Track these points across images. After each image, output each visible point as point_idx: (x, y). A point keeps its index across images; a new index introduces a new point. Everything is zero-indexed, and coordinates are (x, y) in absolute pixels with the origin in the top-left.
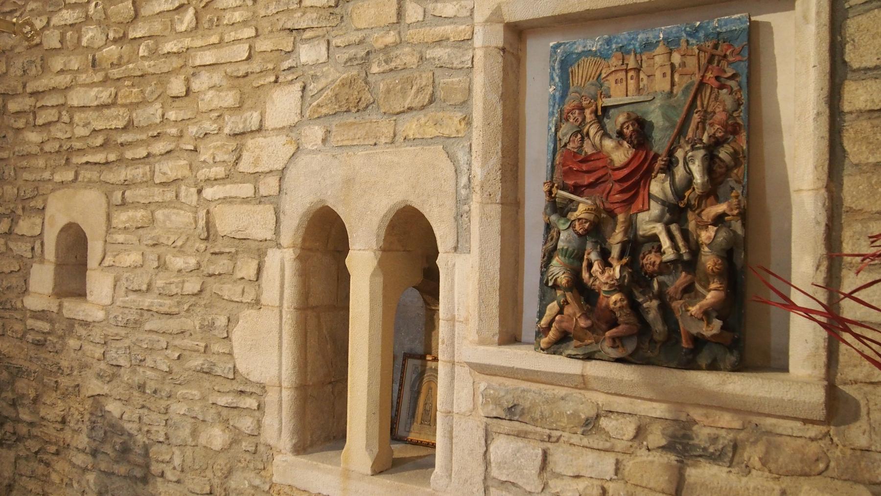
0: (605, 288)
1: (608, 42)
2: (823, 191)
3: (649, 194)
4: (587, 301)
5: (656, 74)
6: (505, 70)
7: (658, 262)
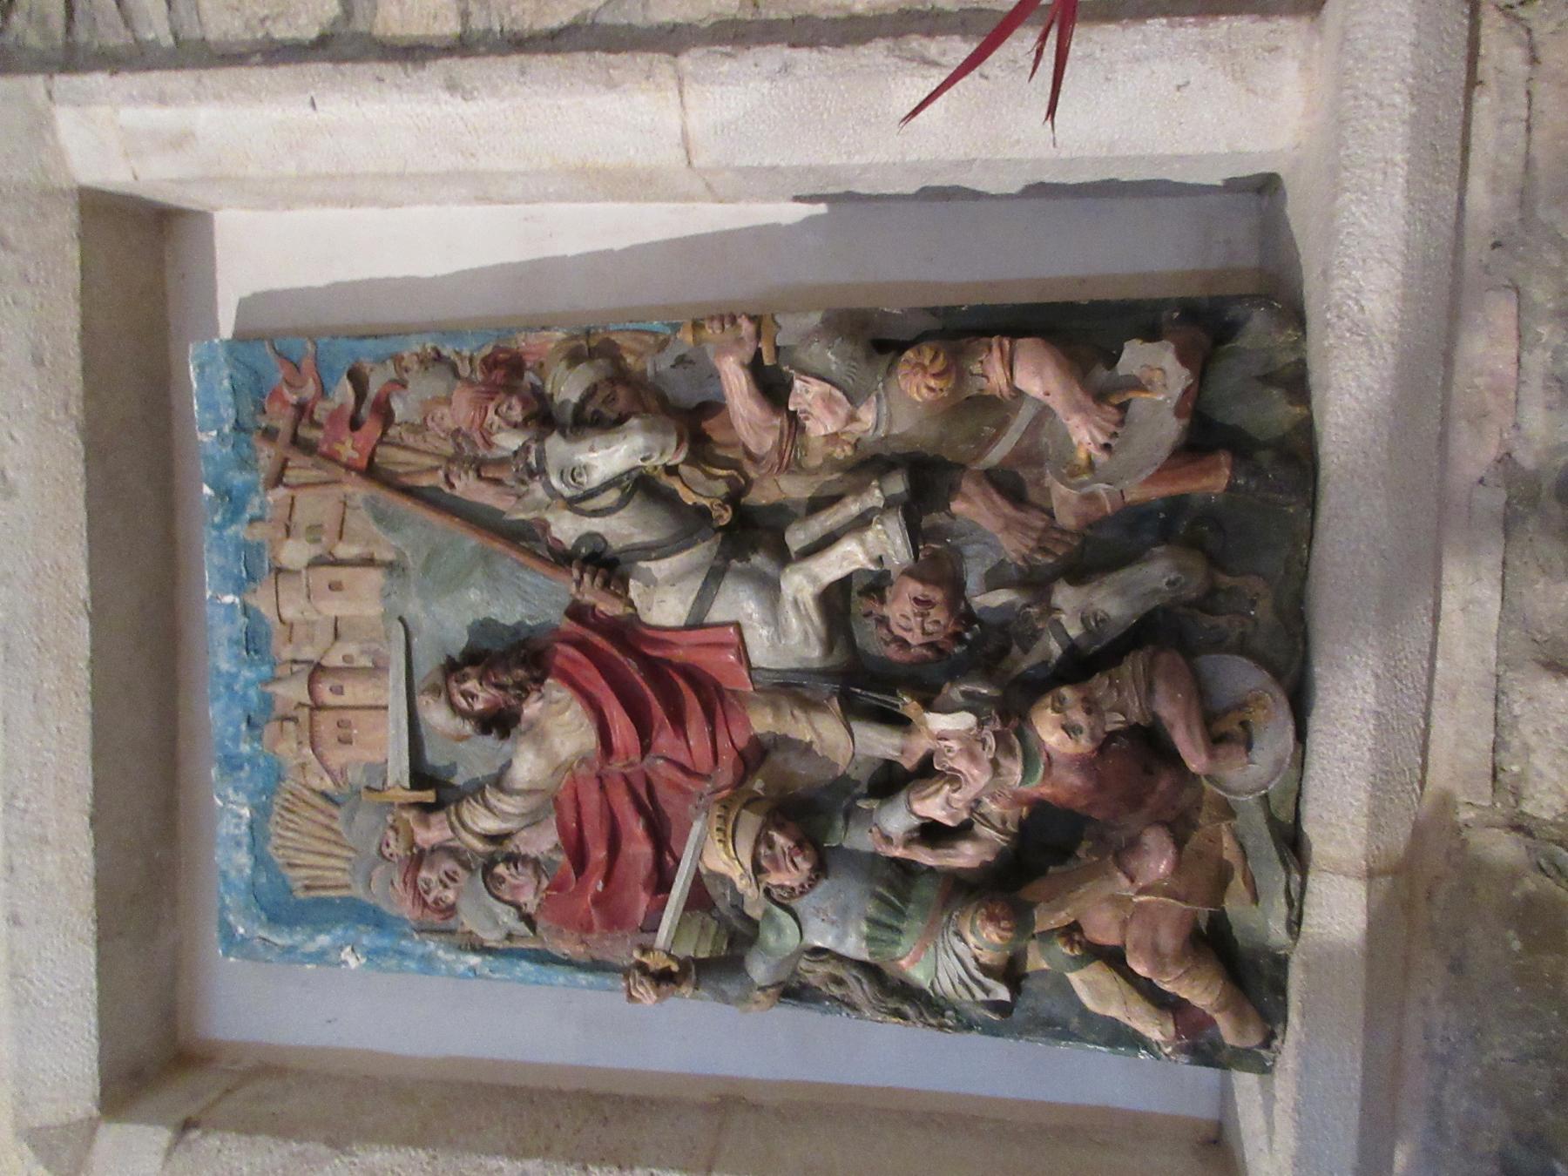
0: (1014, 770)
1: (232, 764)
2: (686, 61)
3: (688, 627)
4: (1064, 853)
5: (333, 614)
6: (248, 1127)
7: (914, 588)
